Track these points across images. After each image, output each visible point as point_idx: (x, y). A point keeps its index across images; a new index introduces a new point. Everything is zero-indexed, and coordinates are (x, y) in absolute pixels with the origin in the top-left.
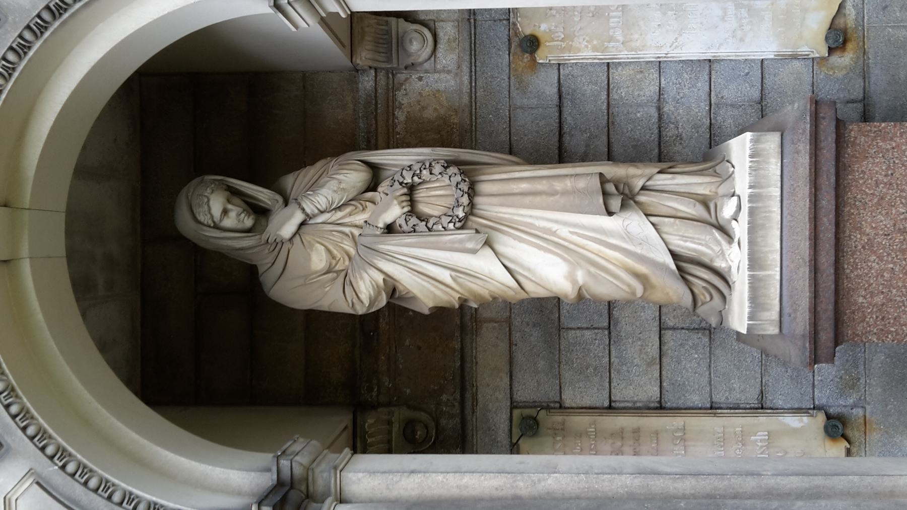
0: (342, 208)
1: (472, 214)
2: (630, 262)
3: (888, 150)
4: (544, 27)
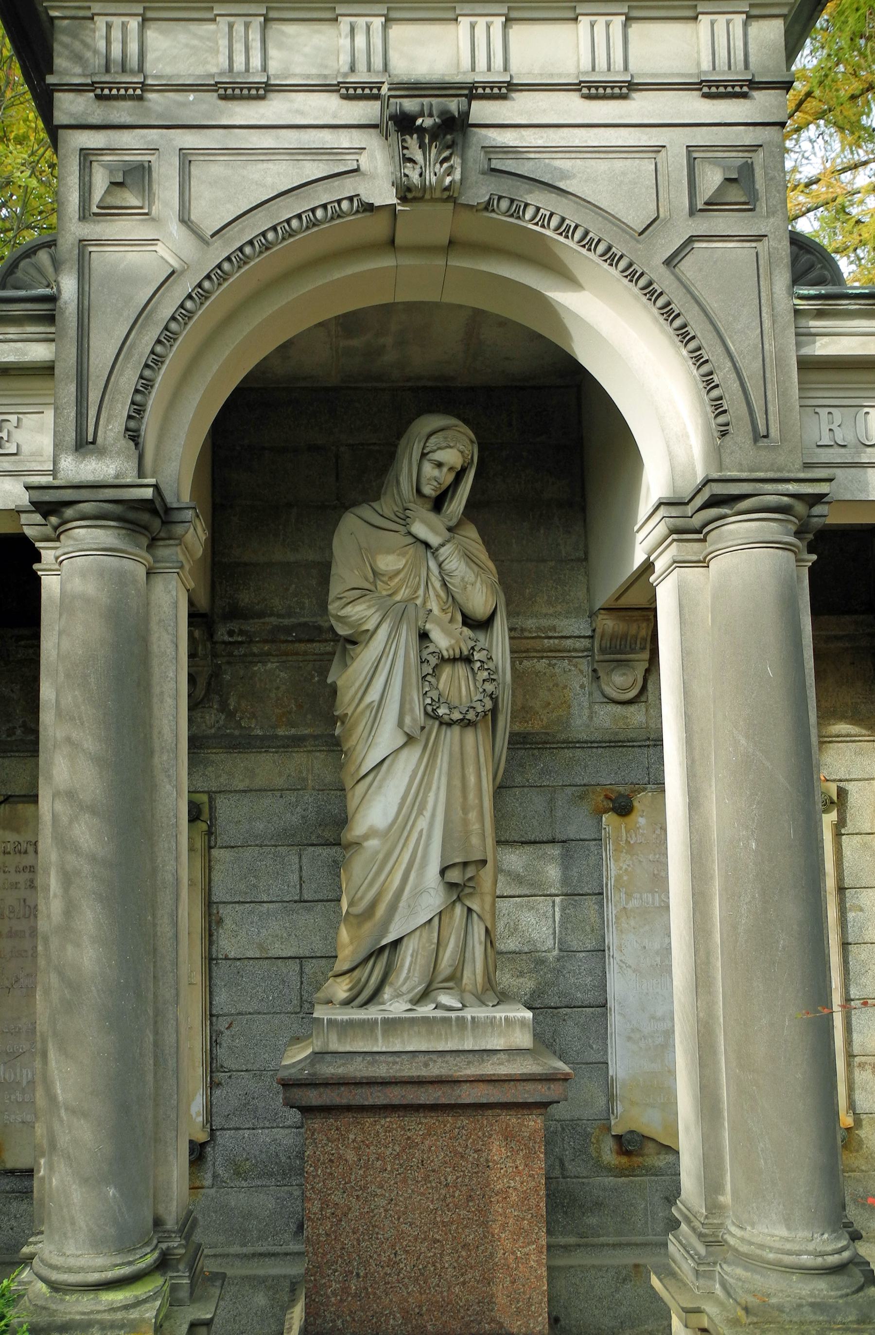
0: (444, 588)
1: (441, 724)
2: (388, 897)
3: (514, 1161)
4: (642, 821)
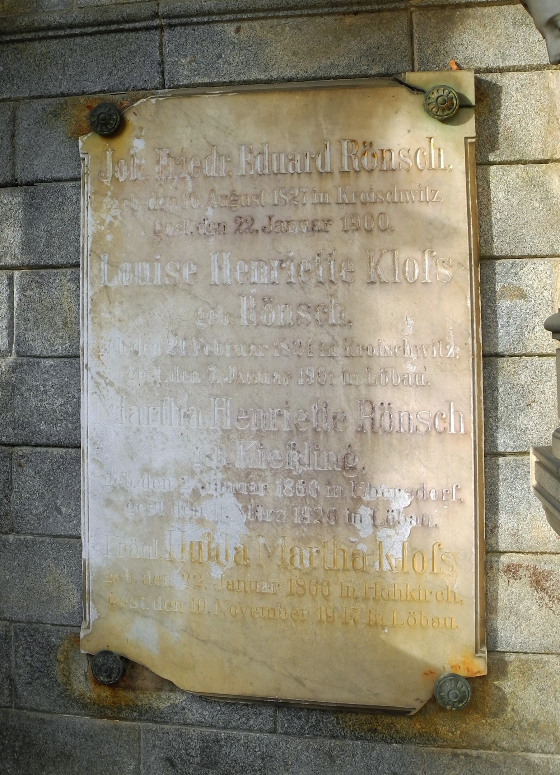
4: (139, 145)
